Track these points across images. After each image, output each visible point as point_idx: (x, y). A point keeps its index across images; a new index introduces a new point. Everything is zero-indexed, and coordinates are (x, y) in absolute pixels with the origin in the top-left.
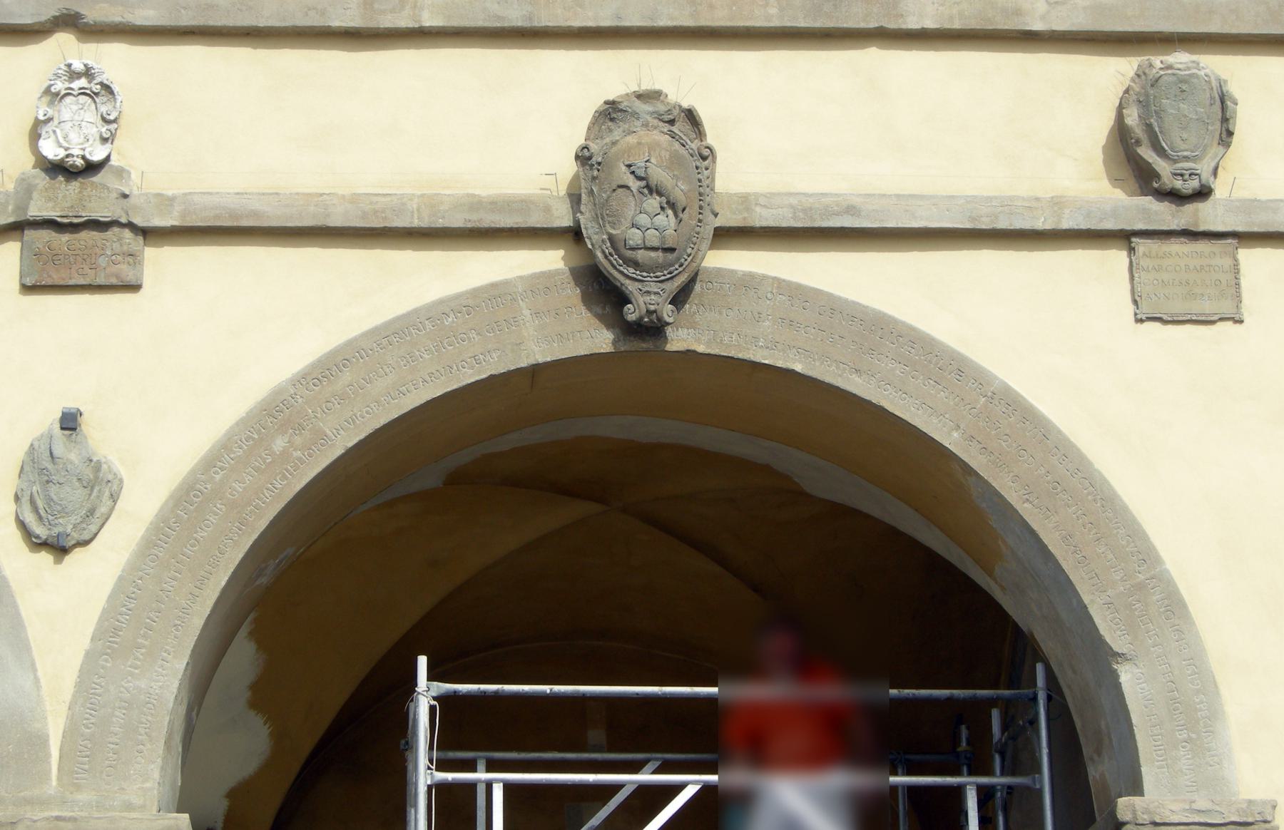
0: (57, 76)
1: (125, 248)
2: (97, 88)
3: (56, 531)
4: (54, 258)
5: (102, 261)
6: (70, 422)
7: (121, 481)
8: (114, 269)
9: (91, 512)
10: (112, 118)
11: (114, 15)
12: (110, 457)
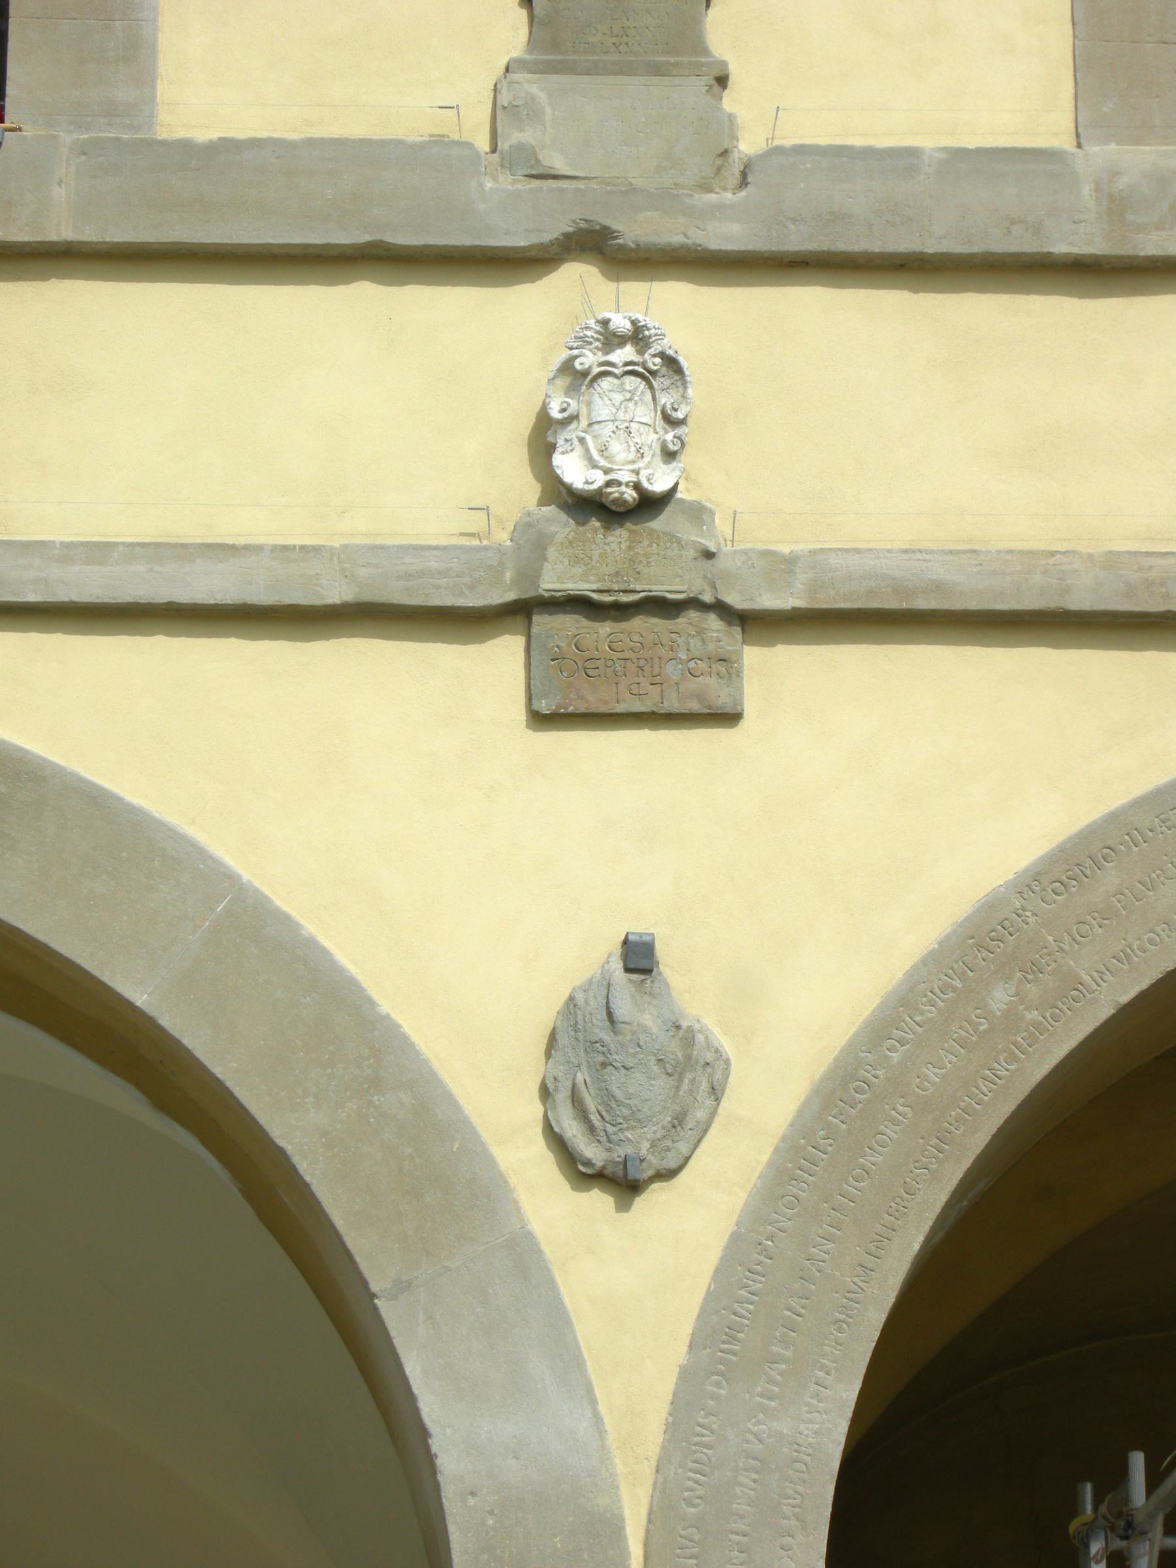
0: (584, 342)
1: (711, 647)
2: (655, 363)
3: (620, 1153)
4: (587, 665)
5: (672, 670)
6: (638, 958)
7: (727, 1062)
8: (693, 685)
9: (679, 1120)
10: (680, 415)
11: (670, 231)
12: (705, 1021)
